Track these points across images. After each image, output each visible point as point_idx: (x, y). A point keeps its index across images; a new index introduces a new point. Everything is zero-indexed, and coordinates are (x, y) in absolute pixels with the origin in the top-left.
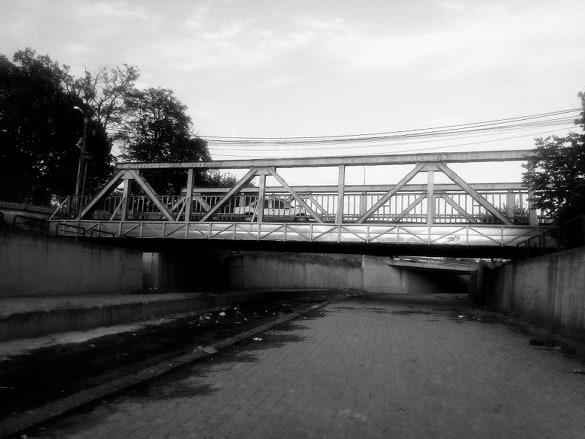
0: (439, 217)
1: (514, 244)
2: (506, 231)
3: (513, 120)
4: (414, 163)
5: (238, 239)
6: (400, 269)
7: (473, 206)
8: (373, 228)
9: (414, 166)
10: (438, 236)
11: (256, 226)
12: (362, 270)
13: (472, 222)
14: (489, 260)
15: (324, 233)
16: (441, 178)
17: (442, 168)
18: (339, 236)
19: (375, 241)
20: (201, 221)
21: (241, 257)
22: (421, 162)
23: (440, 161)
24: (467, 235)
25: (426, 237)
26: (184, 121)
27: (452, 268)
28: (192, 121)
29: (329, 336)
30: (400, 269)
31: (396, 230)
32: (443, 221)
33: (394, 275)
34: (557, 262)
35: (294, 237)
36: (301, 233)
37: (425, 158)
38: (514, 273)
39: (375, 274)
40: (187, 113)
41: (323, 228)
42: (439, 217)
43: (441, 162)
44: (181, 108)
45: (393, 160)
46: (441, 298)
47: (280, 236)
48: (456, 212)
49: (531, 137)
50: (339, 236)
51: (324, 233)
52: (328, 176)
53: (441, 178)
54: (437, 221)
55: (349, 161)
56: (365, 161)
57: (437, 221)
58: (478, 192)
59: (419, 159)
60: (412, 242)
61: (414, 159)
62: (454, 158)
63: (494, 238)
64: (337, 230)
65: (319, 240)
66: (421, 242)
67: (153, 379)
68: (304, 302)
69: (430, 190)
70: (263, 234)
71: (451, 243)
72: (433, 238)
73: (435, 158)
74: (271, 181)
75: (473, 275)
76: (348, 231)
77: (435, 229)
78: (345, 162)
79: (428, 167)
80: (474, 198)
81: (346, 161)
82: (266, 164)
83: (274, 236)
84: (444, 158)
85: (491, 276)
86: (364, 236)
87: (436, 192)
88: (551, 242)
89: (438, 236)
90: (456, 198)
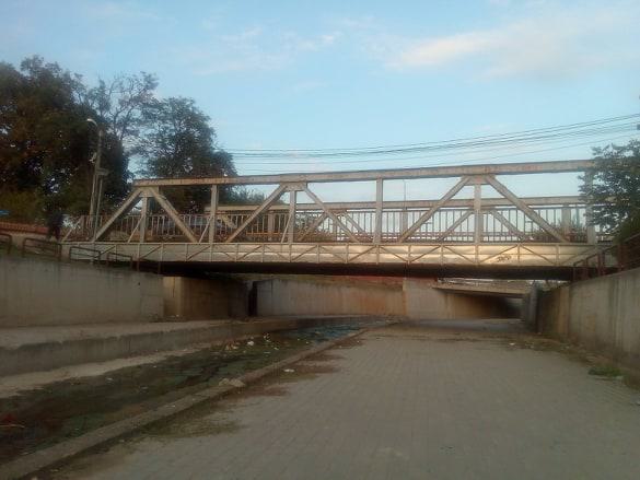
0: (488, 235)
1: (571, 264)
2: (561, 250)
6: (446, 292)
10: (486, 256)
11: (286, 247)
12: (403, 294)
13: (524, 240)
16: (488, 192)
17: (489, 180)
19: (417, 261)
21: (271, 281)
23: (487, 173)
24: (519, 254)
25: (474, 256)
26: (207, 133)
30: (446, 292)
32: (491, 239)
33: (435, 294)
36: (336, 254)
37: (471, 171)
39: (418, 298)
40: (210, 124)
41: (360, 249)
51: (361, 254)
52: (364, 191)
53: (488, 192)
54: (486, 239)
55: (387, 175)
58: (528, 206)
63: (548, 257)
65: (355, 261)
69: (477, 205)
71: (501, 263)
72: (481, 257)
73: (483, 170)
74: (303, 198)
75: (526, 298)
76: (389, 252)
77: (482, 248)
78: (382, 176)
84: (493, 170)
85: (545, 300)
86: (405, 256)
88: (611, 261)
89: (486, 256)
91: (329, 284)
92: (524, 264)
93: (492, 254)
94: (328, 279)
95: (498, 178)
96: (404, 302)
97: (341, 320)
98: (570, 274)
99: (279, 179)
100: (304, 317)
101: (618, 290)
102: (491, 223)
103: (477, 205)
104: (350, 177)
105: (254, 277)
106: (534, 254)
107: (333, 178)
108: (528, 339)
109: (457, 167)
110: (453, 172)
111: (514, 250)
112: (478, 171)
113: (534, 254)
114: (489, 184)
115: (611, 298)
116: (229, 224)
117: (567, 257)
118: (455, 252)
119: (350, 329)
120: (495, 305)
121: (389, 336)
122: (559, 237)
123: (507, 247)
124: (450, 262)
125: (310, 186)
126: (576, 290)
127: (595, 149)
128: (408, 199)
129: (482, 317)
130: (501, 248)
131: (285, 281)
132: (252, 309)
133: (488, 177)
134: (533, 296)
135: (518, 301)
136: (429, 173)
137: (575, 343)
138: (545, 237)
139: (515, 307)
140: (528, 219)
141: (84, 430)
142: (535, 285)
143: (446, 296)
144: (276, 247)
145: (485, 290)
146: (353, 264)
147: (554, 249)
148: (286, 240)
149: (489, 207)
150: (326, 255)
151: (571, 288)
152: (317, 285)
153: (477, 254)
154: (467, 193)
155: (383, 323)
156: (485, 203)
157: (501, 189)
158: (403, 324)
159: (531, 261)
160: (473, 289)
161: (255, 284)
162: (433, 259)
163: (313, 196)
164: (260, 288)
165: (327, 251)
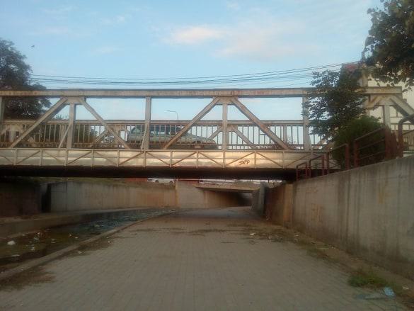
0: (232, 145)
1: (294, 166)
2: (287, 155)
3: (288, 72)
4: (211, 97)
5: (44, 164)
6: (204, 190)
7: (259, 135)
8: (176, 154)
9: (211, 100)
10: (231, 161)
11: (63, 152)
12: (176, 191)
13: (254, 148)
14: (267, 181)
15: (130, 159)
16: (234, 114)
17: (235, 102)
18: (145, 162)
19: (177, 165)
20: (9, 148)
21: (66, 183)
22: (218, 96)
23: (231, 96)
24: (255, 159)
25: (222, 161)
26: (24, 68)
27: (239, 188)
28: (32, 68)
29: (126, 252)
30: (204, 190)
31: (195, 155)
32: (234, 147)
33: (199, 194)
34: (349, 180)
35: (101, 162)
36: (108, 158)
37: (221, 93)
38: (295, 192)
39: (188, 195)
40: (26, 62)
41: (129, 154)
42: (232, 145)
43: (234, 96)
44: (21, 57)
45: (193, 94)
46: (232, 211)
47: (88, 161)
48: (240, 141)
49: (310, 72)
50: (145, 162)
51: (130, 159)
52: (133, 110)
53: (234, 114)
54: (230, 147)
55: (155, 94)
56: (169, 94)
57: (230, 147)
58: (265, 126)
59: (216, 93)
60: (210, 166)
61: (212, 93)
62: (245, 93)
63: (277, 161)
64: (143, 155)
65: (125, 165)
66: (217, 166)
67: (71, 251)
68: (88, 228)
69: (225, 124)
70: (70, 159)
71: (242, 166)
72: (227, 161)
73: (229, 93)
74: (83, 114)
75: (256, 193)
76: (154, 157)
77: (228, 154)
78: (150, 95)
79: (222, 101)
80: (260, 128)
81: (152, 94)
82: (78, 93)
83: (81, 161)
84: (236, 93)
85: (271, 196)
86: (167, 160)
87: (229, 125)
88: (333, 164)
89: (231, 161)
90: (240, 141)
91: (120, 185)
92: (259, 167)
93: (236, 159)
94: (120, 181)
95: (241, 100)
96: (176, 197)
97: (125, 213)
98: (289, 175)
99: (60, 93)
100: (89, 212)
101: (349, 186)
102: (234, 138)
103: (225, 124)
104: (123, 94)
105: (52, 180)
106: (267, 159)
107: (109, 94)
108: (262, 226)
109: (210, 90)
110: (207, 93)
111: (252, 156)
112: (225, 93)
113: (267, 159)
114: (234, 104)
115: (340, 200)
116: (22, 131)
117: (290, 161)
118: (207, 157)
119: (130, 220)
120: (234, 198)
121: (149, 230)
122: (283, 146)
123: (247, 153)
124: (203, 165)
125: (88, 100)
126: (300, 187)
127: (314, 73)
128: (180, 119)
129: (227, 206)
130: (242, 154)
131: (80, 183)
132: (46, 204)
133: (233, 99)
134: (262, 192)
135: (249, 195)
136: (188, 94)
137: (301, 231)
138: (277, 146)
139: (260, 200)
140: (262, 133)
141: (63, 248)
142: (157, 181)
143: (406, 100)
144: (53, 152)
145: (229, 188)
146: (123, 167)
147: (281, 155)
148: (65, 146)
149: (233, 125)
150: (101, 159)
151: (295, 187)
152: (109, 186)
153: (224, 158)
154: (216, 114)
155: (160, 213)
156: (230, 123)
157: (243, 109)
158: (172, 215)
159: (263, 164)
160: (222, 187)
161: (49, 186)
162: (190, 163)
163: (92, 110)
164: (53, 189)
165: (101, 156)
